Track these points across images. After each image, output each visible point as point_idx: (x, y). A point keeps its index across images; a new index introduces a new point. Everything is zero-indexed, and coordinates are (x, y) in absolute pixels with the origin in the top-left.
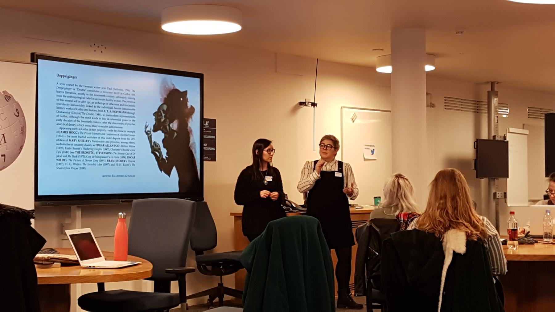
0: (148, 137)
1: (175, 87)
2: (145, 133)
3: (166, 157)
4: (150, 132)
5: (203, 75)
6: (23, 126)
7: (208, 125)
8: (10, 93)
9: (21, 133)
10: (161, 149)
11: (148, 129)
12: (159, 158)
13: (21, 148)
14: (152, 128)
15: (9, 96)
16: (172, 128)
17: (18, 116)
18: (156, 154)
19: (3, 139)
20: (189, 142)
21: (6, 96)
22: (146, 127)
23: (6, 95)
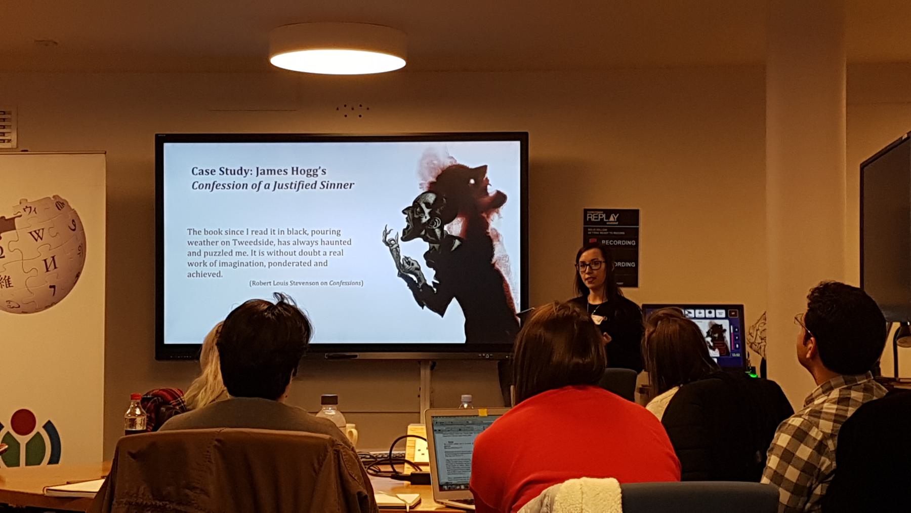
0: (391, 251)
1: (456, 161)
2: (384, 244)
3: (434, 283)
4: (396, 241)
5: (526, 134)
6: (82, 244)
7: (615, 222)
8: (63, 198)
9: (78, 254)
10: (422, 269)
11: (388, 237)
12: (418, 284)
13: (78, 276)
14: (401, 235)
15: (61, 202)
16: (449, 233)
17: (74, 230)
18: (412, 279)
19: (53, 263)
20: (492, 255)
21: (57, 202)
22: (386, 234)
23: (57, 200)
